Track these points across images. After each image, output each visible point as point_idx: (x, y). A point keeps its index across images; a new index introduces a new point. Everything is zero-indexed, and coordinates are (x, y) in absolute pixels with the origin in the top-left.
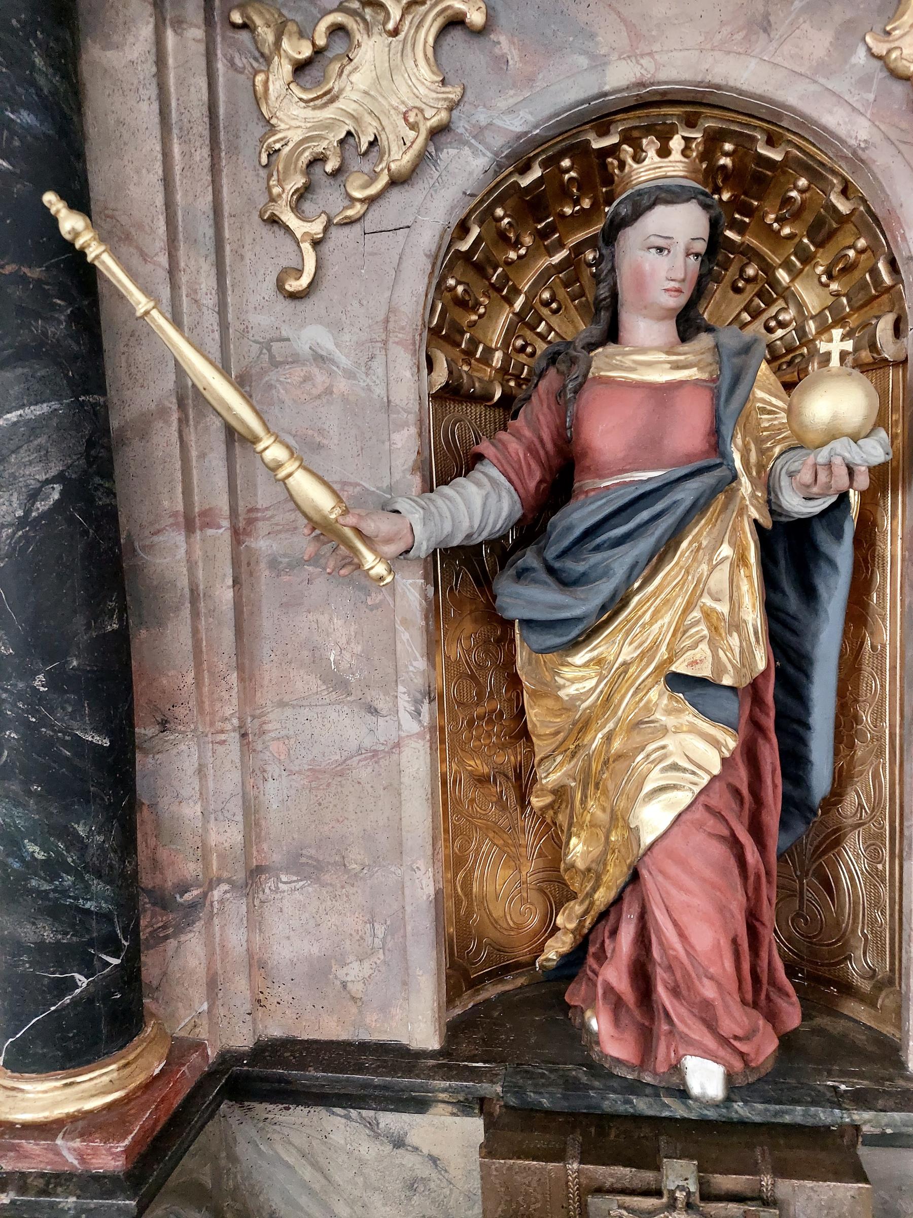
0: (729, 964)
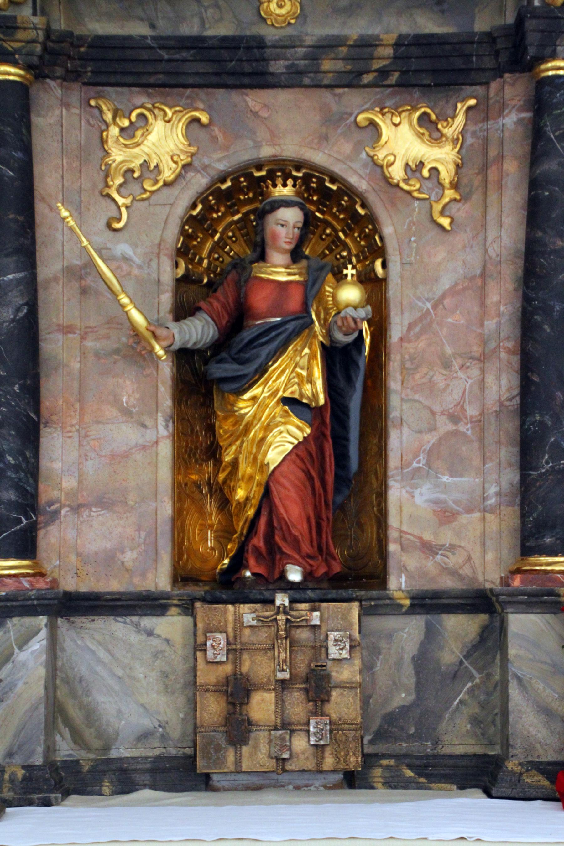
0: (305, 526)
